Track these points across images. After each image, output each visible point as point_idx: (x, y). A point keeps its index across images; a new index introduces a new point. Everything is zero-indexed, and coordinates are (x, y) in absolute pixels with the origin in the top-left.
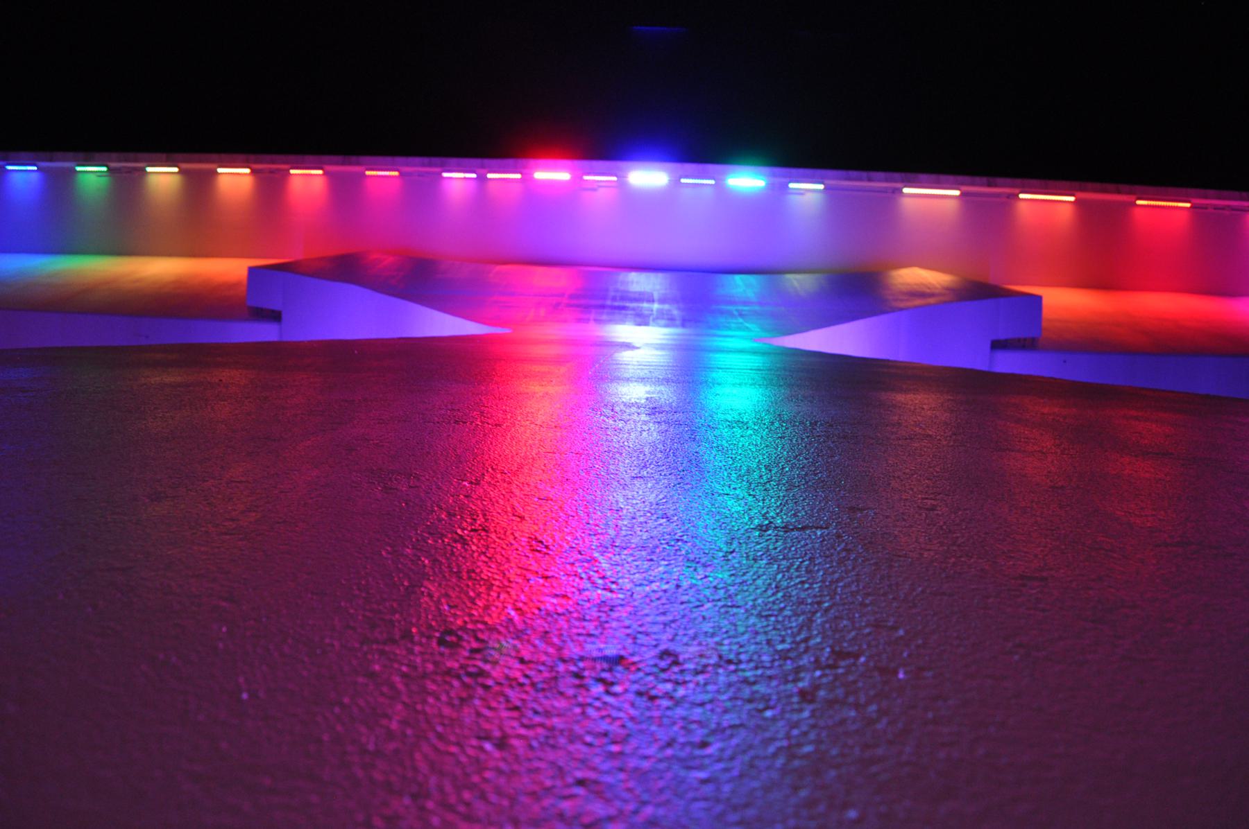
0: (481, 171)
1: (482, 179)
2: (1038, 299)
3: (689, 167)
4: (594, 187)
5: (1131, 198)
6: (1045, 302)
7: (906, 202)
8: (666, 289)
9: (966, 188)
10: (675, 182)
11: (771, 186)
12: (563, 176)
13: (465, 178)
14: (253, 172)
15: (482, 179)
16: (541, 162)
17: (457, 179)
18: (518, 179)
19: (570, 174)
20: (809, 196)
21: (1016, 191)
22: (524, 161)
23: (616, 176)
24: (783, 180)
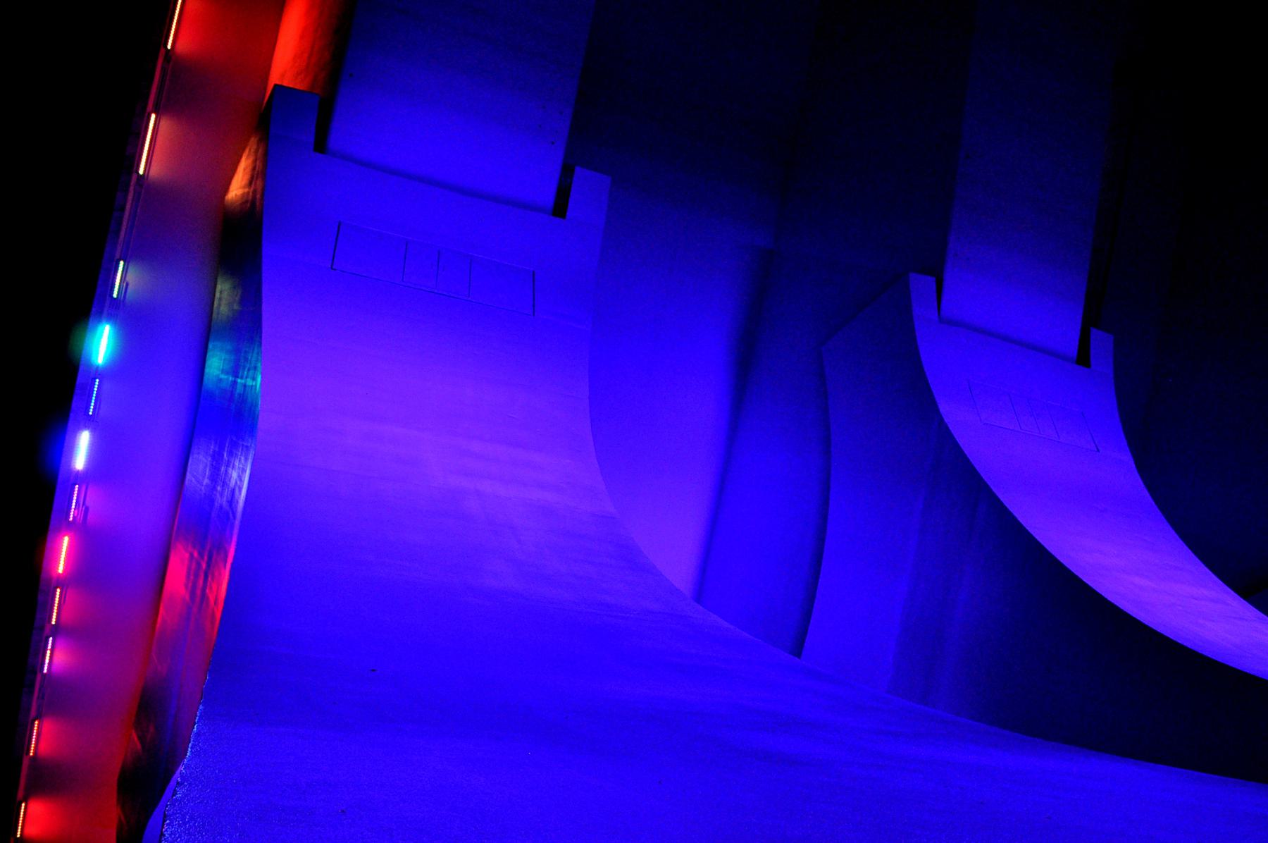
0: (47, 630)
1: (55, 631)
2: (275, 85)
3: (75, 403)
4: (84, 509)
5: (25, 763)
6: (278, 83)
7: (181, 48)
8: (223, 371)
9: (150, 106)
10: (90, 422)
11: (111, 317)
12: (84, 441)
13: (52, 650)
14: (39, 717)
15: (55, 631)
16: (64, 460)
17: (53, 657)
18: (124, 265)
19: (99, 319)
20: (130, 278)
21: (162, 51)
22: (61, 478)
23: (95, 379)
24: (107, 304)
